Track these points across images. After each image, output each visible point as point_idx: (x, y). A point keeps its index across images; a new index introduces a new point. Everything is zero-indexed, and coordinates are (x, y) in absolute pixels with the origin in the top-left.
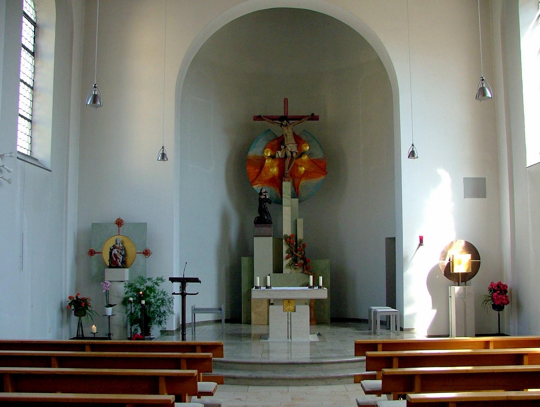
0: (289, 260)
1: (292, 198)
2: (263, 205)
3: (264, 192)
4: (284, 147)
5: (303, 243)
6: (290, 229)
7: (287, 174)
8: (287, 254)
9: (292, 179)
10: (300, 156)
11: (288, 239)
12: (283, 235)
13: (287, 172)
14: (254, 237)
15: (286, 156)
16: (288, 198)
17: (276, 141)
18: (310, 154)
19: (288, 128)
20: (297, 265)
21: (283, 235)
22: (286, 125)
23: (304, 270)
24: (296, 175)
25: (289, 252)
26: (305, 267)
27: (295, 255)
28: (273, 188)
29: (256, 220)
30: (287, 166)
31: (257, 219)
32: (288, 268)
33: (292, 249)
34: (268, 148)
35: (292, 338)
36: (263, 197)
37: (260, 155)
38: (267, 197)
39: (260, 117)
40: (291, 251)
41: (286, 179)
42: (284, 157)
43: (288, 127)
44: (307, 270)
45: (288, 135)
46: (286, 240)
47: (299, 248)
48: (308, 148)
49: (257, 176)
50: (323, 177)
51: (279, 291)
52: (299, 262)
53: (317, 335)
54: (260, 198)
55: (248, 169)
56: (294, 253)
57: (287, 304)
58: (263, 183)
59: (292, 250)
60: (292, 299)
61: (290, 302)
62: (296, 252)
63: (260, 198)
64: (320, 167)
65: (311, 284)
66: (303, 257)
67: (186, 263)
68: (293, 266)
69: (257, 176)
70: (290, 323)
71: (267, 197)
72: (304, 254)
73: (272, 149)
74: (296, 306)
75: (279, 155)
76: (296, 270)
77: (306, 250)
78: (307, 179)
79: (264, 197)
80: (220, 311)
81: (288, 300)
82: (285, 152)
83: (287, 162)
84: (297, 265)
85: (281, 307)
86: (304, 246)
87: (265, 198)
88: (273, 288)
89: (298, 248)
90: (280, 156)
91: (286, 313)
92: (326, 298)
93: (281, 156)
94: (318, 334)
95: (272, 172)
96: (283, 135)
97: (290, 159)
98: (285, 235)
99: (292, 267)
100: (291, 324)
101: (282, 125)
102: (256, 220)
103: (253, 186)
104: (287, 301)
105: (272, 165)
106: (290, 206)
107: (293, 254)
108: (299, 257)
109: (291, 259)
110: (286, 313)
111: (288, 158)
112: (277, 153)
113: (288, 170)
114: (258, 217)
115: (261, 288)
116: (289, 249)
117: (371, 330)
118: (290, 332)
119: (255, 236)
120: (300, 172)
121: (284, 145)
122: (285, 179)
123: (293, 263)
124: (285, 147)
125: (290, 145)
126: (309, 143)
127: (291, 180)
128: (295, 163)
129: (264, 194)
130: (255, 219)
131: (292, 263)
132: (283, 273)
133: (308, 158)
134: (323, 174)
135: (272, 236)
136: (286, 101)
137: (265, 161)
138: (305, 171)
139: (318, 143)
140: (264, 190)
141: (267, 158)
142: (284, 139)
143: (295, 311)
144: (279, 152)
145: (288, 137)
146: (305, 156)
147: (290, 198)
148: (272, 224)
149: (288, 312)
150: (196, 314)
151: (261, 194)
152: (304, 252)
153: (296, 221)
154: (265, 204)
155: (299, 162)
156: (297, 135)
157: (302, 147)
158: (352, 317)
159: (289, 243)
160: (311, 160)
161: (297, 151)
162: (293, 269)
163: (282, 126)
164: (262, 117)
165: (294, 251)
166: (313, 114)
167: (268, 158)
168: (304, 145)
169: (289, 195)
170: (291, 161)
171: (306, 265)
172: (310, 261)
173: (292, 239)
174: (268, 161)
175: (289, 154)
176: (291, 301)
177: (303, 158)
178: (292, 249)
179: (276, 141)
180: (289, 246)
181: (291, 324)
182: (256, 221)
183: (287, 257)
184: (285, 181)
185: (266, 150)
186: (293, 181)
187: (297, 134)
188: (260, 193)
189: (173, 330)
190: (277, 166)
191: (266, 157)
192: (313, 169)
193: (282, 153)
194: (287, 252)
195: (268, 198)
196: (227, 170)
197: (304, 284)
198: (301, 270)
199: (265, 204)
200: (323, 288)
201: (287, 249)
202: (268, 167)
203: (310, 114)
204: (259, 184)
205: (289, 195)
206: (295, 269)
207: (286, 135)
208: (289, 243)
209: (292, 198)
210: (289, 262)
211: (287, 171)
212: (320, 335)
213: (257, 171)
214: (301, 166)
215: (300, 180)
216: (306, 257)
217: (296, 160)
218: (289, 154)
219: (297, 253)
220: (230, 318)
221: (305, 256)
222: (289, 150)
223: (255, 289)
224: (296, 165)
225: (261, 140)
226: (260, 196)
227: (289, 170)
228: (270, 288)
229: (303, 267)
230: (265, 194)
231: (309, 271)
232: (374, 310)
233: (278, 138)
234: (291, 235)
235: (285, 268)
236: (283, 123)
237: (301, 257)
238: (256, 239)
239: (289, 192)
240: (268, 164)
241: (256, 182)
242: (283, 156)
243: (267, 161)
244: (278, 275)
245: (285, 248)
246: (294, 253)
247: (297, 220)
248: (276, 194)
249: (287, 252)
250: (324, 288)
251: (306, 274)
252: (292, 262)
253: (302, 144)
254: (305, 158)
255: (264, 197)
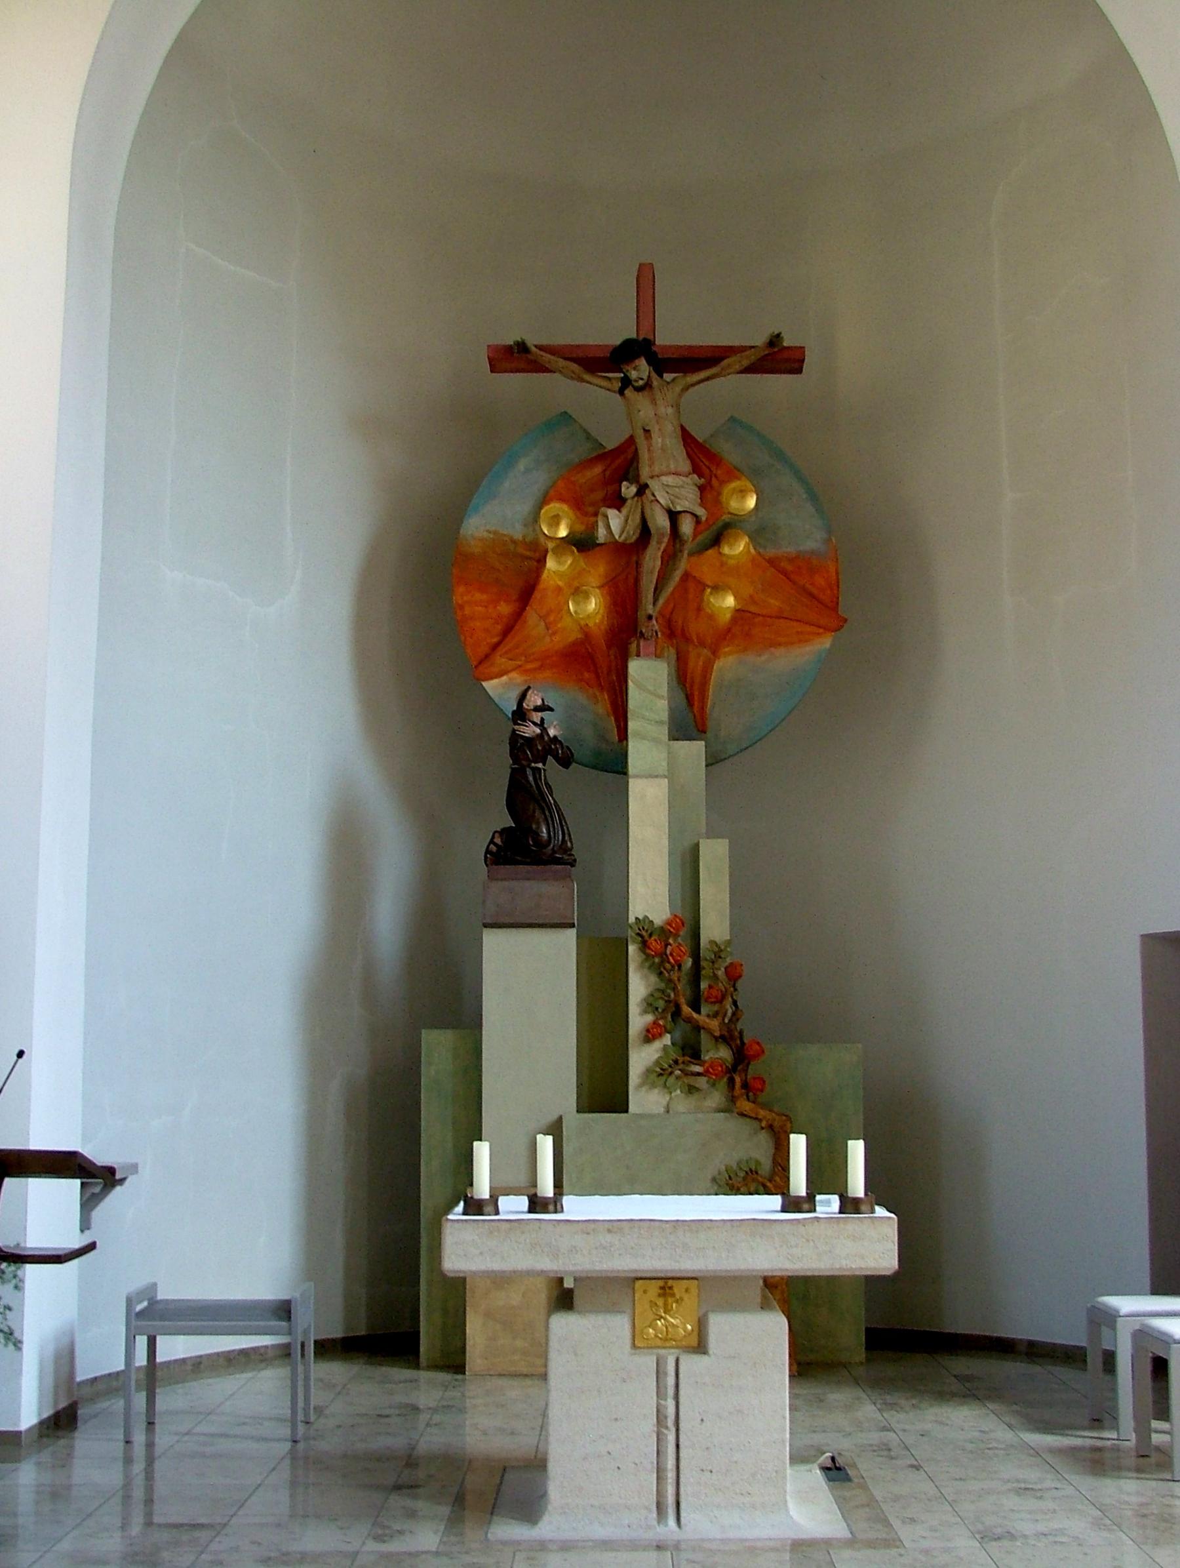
0: (657, 1045)
1: (673, 737)
2: (529, 772)
3: (537, 709)
4: (633, 489)
5: (729, 960)
6: (663, 890)
7: (650, 617)
8: (649, 1018)
9: (673, 651)
10: (716, 541)
11: (654, 943)
12: (632, 920)
13: (650, 610)
14: (485, 929)
15: (645, 532)
16: (656, 741)
17: (598, 470)
18: (760, 532)
19: (654, 402)
20: (698, 1069)
21: (632, 920)
22: (648, 386)
23: (733, 1099)
24: (696, 628)
25: (661, 1004)
26: (738, 1079)
27: (689, 1020)
28: (582, 699)
29: (495, 844)
30: (648, 583)
31: (498, 840)
32: (653, 1086)
33: (674, 989)
34: (562, 500)
35: (683, 1514)
36: (530, 731)
37: (518, 536)
38: (552, 732)
39: (522, 347)
40: (668, 1002)
41: (642, 643)
42: (634, 538)
43: (658, 396)
44: (748, 1099)
45: (655, 435)
46: (644, 945)
47: (710, 987)
48: (751, 502)
49: (507, 631)
50: (825, 642)
51: (609, 1231)
52: (706, 1057)
53: (825, 1469)
54: (514, 737)
55: (457, 599)
56: (686, 1010)
57: (653, 1304)
58: (529, 666)
59: (672, 995)
60: (678, 1275)
61: (676, 1290)
62: (696, 1006)
63: (514, 737)
64: (812, 596)
65: (799, 1183)
66: (730, 1031)
67: (20, 1054)
68: (678, 1078)
69: (507, 631)
70: (670, 1422)
71: (552, 732)
72: (734, 1014)
73: (578, 504)
74: (705, 1315)
75: (613, 528)
76: (696, 1096)
77: (745, 991)
78: (745, 650)
79: (538, 731)
80: (284, 1324)
81: (661, 1283)
82: (643, 513)
83: (652, 560)
84: (698, 1069)
85: (619, 1325)
86: (733, 975)
87: (540, 736)
88: (576, 1207)
89: (704, 985)
90: (617, 537)
91: (648, 1362)
92: (888, 1273)
93: (622, 532)
94: (829, 1464)
95: (576, 612)
96: (631, 440)
97: (663, 546)
98: (637, 918)
99: (671, 1080)
100: (677, 1430)
101: (626, 382)
102: (495, 844)
103: (484, 684)
104: (654, 1288)
105: (576, 584)
106: (666, 777)
107: (677, 1013)
108: (709, 1032)
109: (667, 1039)
110: (648, 1362)
111: (653, 543)
112: (600, 524)
113: (657, 591)
114: (504, 832)
115: (497, 1213)
116: (658, 990)
117: (1115, 1427)
118: (671, 1475)
119: (486, 926)
120: (711, 617)
121: (636, 479)
122: (638, 646)
123: (681, 1059)
124: (642, 489)
125: (664, 479)
126: (757, 478)
127: (672, 653)
128: (686, 576)
129: (536, 717)
130: (492, 842)
131: (676, 1062)
132: (626, 1111)
133: (752, 551)
134: (827, 629)
135: (572, 926)
136: (645, 279)
137: (542, 561)
138: (740, 614)
139: (801, 479)
140: (534, 699)
141: (552, 550)
142: (635, 457)
143: (700, 1347)
144: (612, 513)
145: (657, 440)
146: (736, 540)
147: (665, 738)
148: (573, 864)
149: (662, 1352)
150: (158, 1338)
151: (520, 715)
152: (735, 1003)
153: (696, 848)
154: (540, 765)
155: (705, 568)
156: (700, 440)
157: (724, 499)
158: (961, 1322)
159: (657, 960)
160: (772, 562)
161: (701, 512)
162: (678, 1092)
163: (626, 392)
164: (533, 349)
165: (682, 1001)
166: (775, 341)
167: (557, 547)
168: (734, 489)
169: (661, 723)
170: (670, 558)
171: (746, 1071)
172: (763, 1052)
173: (675, 941)
174: (559, 563)
175: (661, 521)
176: (678, 1288)
177: (726, 550)
178: (674, 989)
179: (598, 470)
180: (661, 974)
181: (677, 1430)
182: (493, 848)
183: (648, 1031)
184: (638, 655)
185: (546, 508)
186: (678, 659)
187: (700, 435)
188: (514, 713)
189: (18, 1434)
190: (599, 587)
191: (550, 545)
192: (775, 603)
193: (626, 521)
194: (649, 1005)
195: (555, 737)
196: (362, 623)
197: (735, 1167)
198: (716, 1098)
199: (540, 765)
200: (873, 1211)
201: (650, 989)
202: (559, 589)
203: (759, 339)
204: (514, 675)
205: (661, 723)
206: (691, 1090)
207: (647, 432)
208: (659, 963)
209: (673, 737)
210: (660, 1057)
211: (648, 607)
212: (839, 1469)
213: (505, 609)
214: (716, 588)
215: (715, 653)
216: (741, 1033)
217: (694, 559)
218: (661, 521)
219: (698, 1012)
220: (363, 1333)
221: (739, 1026)
222: (662, 501)
223: (465, 1213)
224: (693, 587)
225: (522, 465)
226: (516, 723)
227: (661, 601)
228: (551, 1207)
229: (731, 1082)
230: (542, 720)
231: (759, 1100)
232: (1136, 1324)
233: (604, 457)
234: (669, 923)
235: (641, 1085)
236: (634, 375)
237: (717, 1034)
238: (495, 944)
239: (661, 708)
240: (560, 575)
241: (500, 660)
242: (632, 535)
243: (551, 564)
244: (577, 1300)
245: (639, 986)
246: (686, 1010)
247: (697, 845)
248: (613, 1257)
249: (650, 1005)
250: (880, 1211)
251: (742, 1115)
252: (674, 1056)
253: (723, 483)
254: (738, 548)
255: (538, 731)
